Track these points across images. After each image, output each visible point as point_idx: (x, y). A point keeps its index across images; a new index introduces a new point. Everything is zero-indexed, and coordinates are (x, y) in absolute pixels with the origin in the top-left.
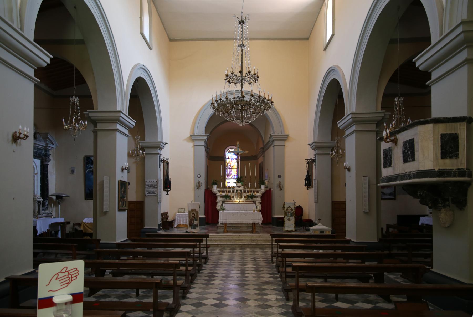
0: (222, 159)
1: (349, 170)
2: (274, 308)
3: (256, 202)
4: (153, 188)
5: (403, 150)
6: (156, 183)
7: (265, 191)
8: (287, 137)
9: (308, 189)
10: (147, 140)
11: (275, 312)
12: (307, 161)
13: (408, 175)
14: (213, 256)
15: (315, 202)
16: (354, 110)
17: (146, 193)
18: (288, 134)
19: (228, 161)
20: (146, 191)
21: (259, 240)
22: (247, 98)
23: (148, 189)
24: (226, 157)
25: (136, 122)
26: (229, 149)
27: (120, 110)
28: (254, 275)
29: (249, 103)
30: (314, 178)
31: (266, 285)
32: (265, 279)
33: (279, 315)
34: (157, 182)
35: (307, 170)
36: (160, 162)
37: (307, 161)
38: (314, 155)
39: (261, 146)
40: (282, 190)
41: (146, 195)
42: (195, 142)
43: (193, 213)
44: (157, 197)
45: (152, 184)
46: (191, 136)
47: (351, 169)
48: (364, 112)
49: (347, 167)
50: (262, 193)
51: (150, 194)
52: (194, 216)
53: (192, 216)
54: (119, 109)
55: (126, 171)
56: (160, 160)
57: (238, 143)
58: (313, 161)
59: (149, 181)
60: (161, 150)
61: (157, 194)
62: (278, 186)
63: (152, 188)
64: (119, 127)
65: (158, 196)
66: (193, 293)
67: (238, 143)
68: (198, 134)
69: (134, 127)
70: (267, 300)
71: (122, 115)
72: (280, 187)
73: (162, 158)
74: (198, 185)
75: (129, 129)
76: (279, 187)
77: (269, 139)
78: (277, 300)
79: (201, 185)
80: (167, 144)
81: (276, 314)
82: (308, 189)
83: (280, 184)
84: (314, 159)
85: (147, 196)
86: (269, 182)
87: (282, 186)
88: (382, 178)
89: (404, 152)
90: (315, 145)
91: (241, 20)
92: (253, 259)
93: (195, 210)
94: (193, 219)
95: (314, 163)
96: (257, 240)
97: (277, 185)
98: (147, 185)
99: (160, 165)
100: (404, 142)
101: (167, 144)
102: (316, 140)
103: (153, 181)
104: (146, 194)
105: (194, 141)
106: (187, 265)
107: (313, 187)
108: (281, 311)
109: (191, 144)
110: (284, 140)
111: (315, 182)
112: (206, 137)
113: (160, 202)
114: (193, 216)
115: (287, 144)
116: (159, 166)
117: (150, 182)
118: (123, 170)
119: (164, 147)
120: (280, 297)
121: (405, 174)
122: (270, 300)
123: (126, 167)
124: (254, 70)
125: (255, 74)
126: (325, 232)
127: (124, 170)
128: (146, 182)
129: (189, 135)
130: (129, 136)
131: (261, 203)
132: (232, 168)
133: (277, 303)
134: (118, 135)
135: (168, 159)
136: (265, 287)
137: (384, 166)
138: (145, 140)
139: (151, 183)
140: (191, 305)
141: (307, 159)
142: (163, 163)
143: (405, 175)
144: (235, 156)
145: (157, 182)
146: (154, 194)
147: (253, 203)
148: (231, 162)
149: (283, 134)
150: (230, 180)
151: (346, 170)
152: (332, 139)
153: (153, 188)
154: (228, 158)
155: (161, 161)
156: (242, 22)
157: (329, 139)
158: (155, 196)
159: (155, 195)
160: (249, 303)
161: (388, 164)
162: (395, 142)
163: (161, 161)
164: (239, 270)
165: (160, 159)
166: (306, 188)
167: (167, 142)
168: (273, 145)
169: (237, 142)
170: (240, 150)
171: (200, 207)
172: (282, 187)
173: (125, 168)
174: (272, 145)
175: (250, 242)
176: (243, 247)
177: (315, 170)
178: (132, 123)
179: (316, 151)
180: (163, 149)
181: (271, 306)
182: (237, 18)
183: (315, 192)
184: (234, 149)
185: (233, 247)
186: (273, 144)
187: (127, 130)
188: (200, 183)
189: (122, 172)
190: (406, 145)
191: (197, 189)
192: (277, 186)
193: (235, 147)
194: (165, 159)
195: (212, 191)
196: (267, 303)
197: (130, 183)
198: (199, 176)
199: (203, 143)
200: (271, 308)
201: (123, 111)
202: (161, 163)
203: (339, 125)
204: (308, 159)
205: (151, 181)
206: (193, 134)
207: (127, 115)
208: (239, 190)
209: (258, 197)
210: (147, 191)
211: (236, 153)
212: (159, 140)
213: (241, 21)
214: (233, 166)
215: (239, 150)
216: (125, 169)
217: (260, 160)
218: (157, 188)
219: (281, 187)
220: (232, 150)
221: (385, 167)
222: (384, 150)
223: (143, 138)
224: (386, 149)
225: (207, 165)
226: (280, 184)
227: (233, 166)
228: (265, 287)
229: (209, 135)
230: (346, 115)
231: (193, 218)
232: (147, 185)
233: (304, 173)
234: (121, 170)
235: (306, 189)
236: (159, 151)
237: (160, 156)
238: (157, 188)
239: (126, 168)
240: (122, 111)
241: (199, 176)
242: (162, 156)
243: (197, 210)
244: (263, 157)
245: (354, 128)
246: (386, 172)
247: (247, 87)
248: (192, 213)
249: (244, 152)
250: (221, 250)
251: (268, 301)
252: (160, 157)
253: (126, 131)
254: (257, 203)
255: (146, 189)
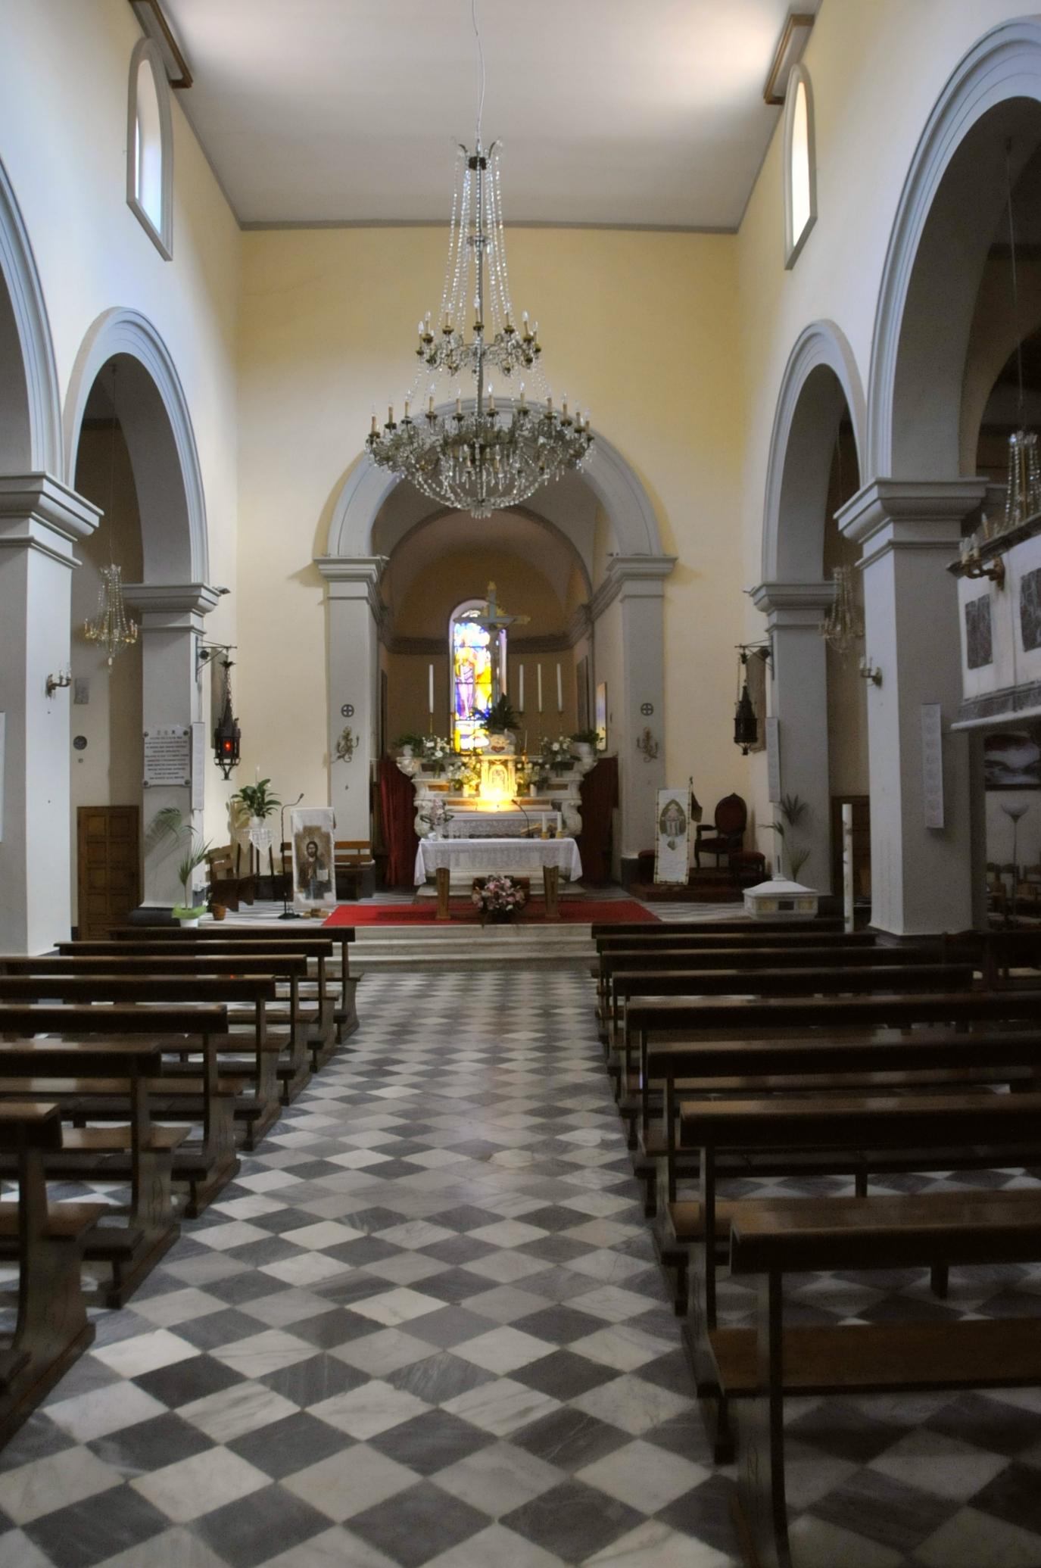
0: (439, 649)
1: (878, 680)
2: (587, 1173)
3: (561, 803)
4: (174, 756)
5: (1023, 605)
6: (186, 738)
7: (595, 764)
8: (670, 565)
9: (745, 753)
10: (150, 579)
11: (591, 1186)
12: (741, 651)
13: (1037, 691)
14: (393, 1002)
15: (771, 801)
16: (886, 472)
17: (148, 776)
18: (674, 555)
19: (461, 654)
20: (146, 768)
21: (569, 943)
22: (504, 422)
23: (153, 761)
24: (454, 640)
25: (102, 512)
26: (466, 611)
27: (40, 470)
28: (535, 1065)
29: (510, 441)
30: (769, 714)
31: (570, 1098)
32: (569, 1078)
33: (600, 1192)
34: (188, 733)
35: (743, 684)
36: (200, 659)
37: (741, 651)
38: (767, 631)
39: (583, 598)
40: (655, 757)
41: (146, 783)
42: (331, 584)
43: (311, 843)
44: (188, 789)
45: (169, 740)
46: (317, 562)
47: (883, 679)
48: (922, 478)
49: (870, 670)
50: (584, 772)
51: (164, 778)
52: (314, 850)
53: (306, 853)
54: (37, 466)
55: (64, 694)
56: (200, 651)
57: (492, 586)
58: (765, 653)
59: (159, 732)
60: (201, 616)
61: (187, 777)
62: (642, 744)
63: (168, 756)
64: (35, 529)
65: (191, 787)
66: (301, 1130)
67: (492, 586)
68: (343, 555)
69: (94, 532)
70: (566, 1147)
71: (47, 487)
72: (650, 747)
73: (205, 644)
74: (343, 743)
75: (76, 540)
76: (645, 747)
77: (608, 573)
78: (605, 1145)
79: (354, 743)
80: (224, 591)
81: (592, 1190)
82: (745, 753)
83: (648, 736)
84: (767, 644)
85: (151, 786)
86: (609, 732)
87: (657, 745)
88: (964, 703)
89: (1024, 613)
90: (769, 595)
91: (474, 155)
92: (541, 1011)
93: (318, 829)
94: (310, 864)
95: (768, 660)
96: (563, 943)
97: (638, 741)
98: (148, 745)
99: (197, 670)
100: (1023, 578)
101: (224, 591)
102: (773, 577)
103: (173, 732)
104: (146, 778)
105: (328, 581)
106: (263, 1020)
107: (763, 747)
108: (612, 1180)
109: (318, 593)
110: (662, 577)
111: (770, 730)
112: (373, 567)
113: (200, 810)
114: (310, 850)
115: (673, 591)
116: (197, 674)
117: (162, 734)
118: (51, 688)
119: (215, 604)
120: (615, 1136)
121: (1029, 687)
122: (578, 1147)
123: (61, 678)
124: (526, 323)
125: (529, 340)
126: (795, 906)
127: (54, 689)
128: (146, 735)
129: (309, 561)
130: (75, 564)
131: (580, 809)
132: (475, 680)
133: (602, 1155)
134: (32, 555)
135: (227, 648)
136: (568, 1103)
137: (969, 660)
138: (141, 581)
139: (163, 738)
140: (288, 1170)
141: (741, 647)
142: (209, 664)
143: (1030, 690)
144: (485, 638)
145: (185, 733)
146: (176, 778)
147: (550, 807)
148: (472, 660)
149: (656, 553)
150: (469, 725)
151: (870, 681)
152: (828, 574)
153: (174, 756)
154: (463, 645)
155: (204, 655)
156: (477, 163)
157: (815, 573)
158: (181, 786)
159: (182, 782)
160: (500, 1157)
161: (981, 655)
162: (998, 576)
163: (204, 655)
164: (481, 1051)
165: (197, 647)
166: (739, 749)
167: (224, 586)
168: (620, 597)
169: (488, 584)
170: (500, 612)
171: (299, 795)
172: (654, 747)
173: (58, 682)
174: (617, 595)
175: (535, 951)
176: (510, 966)
177: (772, 684)
178: (89, 516)
179: (771, 616)
180: (209, 611)
181: (576, 1167)
182: (460, 148)
183: (770, 765)
184: (478, 609)
185: (471, 968)
186: (620, 591)
187: (70, 544)
188: (353, 736)
189: (50, 696)
190: (1029, 587)
191: (339, 757)
192: (638, 746)
193: (483, 604)
194: (220, 649)
195: (399, 765)
196: (567, 1157)
197: (88, 741)
198: (348, 711)
199: (362, 589)
200: (577, 1173)
201: (54, 474)
202: (201, 661)
203: (842, 524)
204: (743, 645)
205: (166, 733)
206: (326, 556)
207: (71, 488)
208: (496, 760)
209: (569, 787)
210: (150, 770)
211: (487, 625)
212: (195, 579)
213: (475, 158)
214: (479, 676)
215: (498, 615)
216: (60, 685)
217: (581, 650)
218: (187, 755)
219: (651, 747)
220: (475, 614)
221: (973, 664)
222: (967, 606)
223: (134, 572)
224: (972, 602)
225: (384, 676)
226: (648, 736)
227: (479, 676)
228: (568, 1103)
229: (383, 560)
230: (863, 489)
231: (311, 860)
232: (148, 745)
233: (734, 697)
234: (44, 688)
235: (741, 755)
236: (193, 620)
237: (197, 639)
238: (187, 755)
239: (61, 681)
240: (48, 474)
241: (348, 711)
242: (205, 637)
243: (324, 830)
244: (588, 639)
245: (888, 534)
246: (977, 683)
247: (496, 387)
248: (307, 841)
249: (515, 620)
250: (424, 983)
251: (571, 1151)
252: (199, 642)
253: (65, 548)
254: (564, 807)
255: (146, 759)
